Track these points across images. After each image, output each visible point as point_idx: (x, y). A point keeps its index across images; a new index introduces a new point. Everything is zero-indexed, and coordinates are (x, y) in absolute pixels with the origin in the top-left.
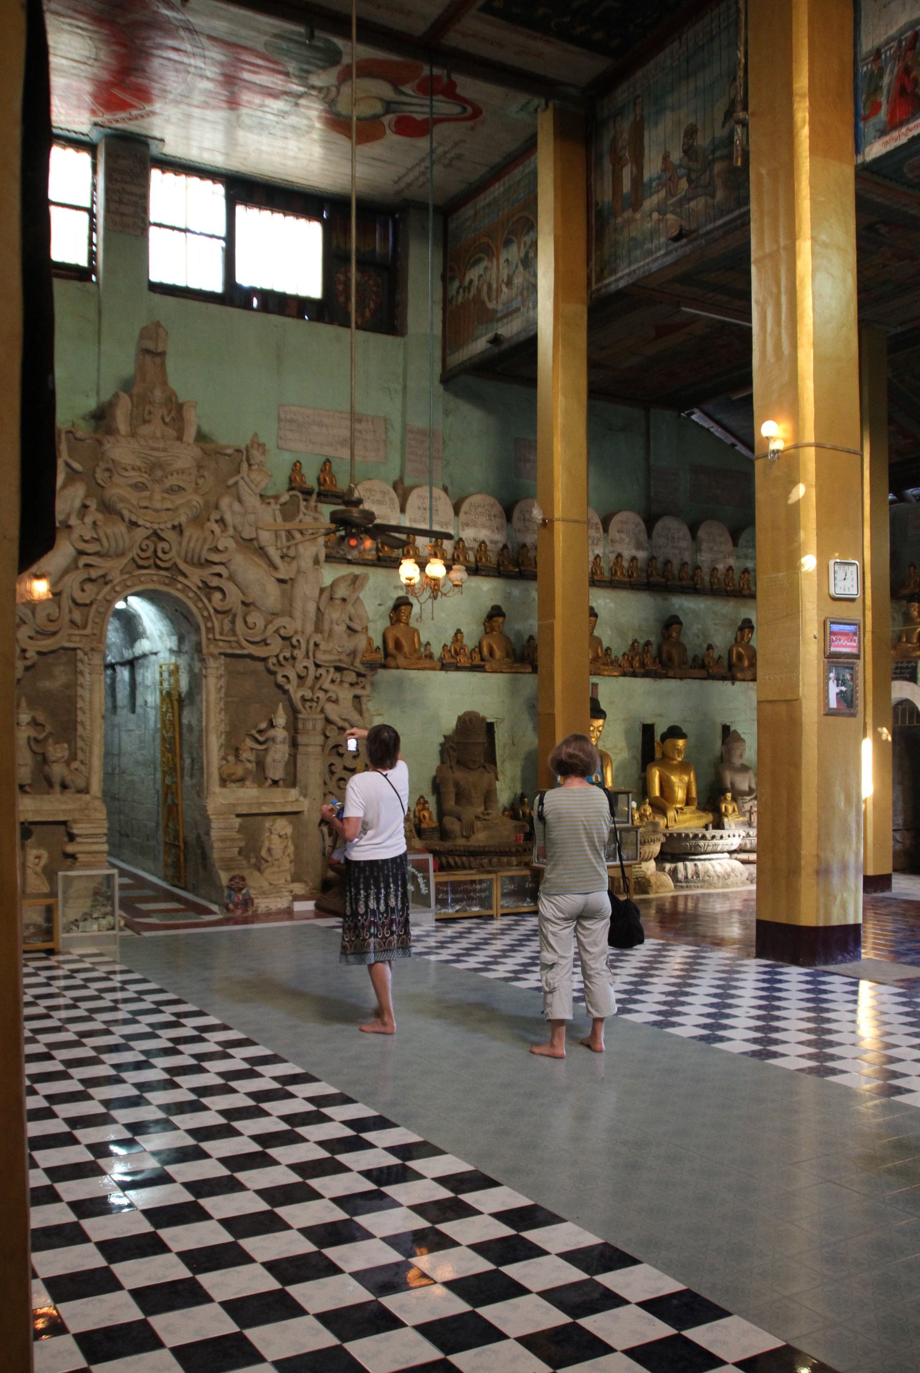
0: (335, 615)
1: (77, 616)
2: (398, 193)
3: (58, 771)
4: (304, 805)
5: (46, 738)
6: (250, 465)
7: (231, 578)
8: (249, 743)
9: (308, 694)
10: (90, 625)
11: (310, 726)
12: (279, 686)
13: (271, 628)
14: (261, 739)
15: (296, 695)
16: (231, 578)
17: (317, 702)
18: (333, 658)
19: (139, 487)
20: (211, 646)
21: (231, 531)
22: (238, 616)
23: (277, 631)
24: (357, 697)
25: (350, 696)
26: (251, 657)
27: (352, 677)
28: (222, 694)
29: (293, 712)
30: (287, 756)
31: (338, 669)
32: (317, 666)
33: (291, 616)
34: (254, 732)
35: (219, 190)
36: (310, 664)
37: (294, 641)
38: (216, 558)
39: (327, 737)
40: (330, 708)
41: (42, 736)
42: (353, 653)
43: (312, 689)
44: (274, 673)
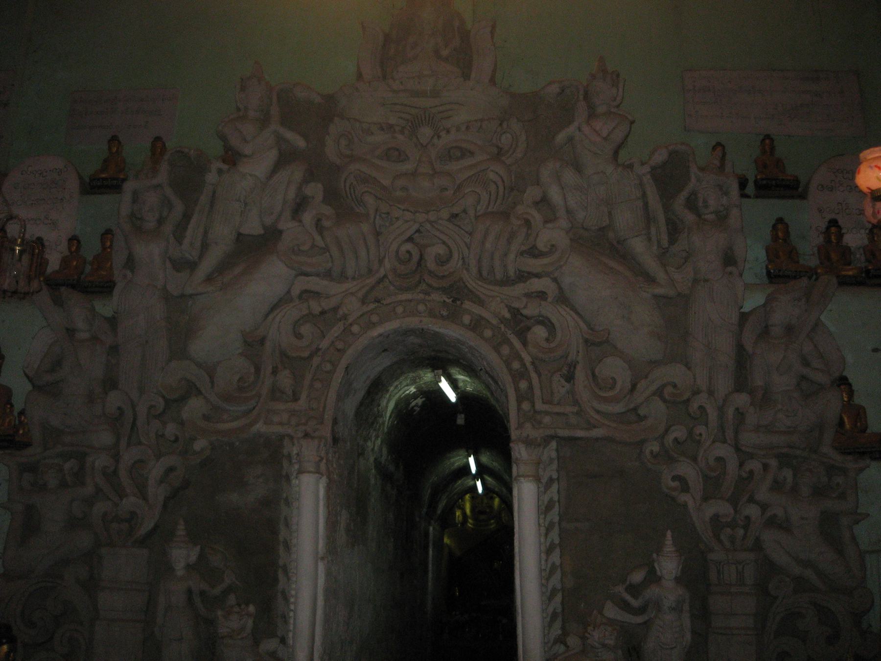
1: (285, 379)
7: (563, 299)
10: (304, 396)
14: (635, 603)
16: (563, 299)
17: (746, 527)
19: (395, 154)
20: (528, 425)
22: (579, 368)
23: (659, 393)
30: (688, 636)
34: (620, 589)
41: (217, 591)
43: (734, 501)
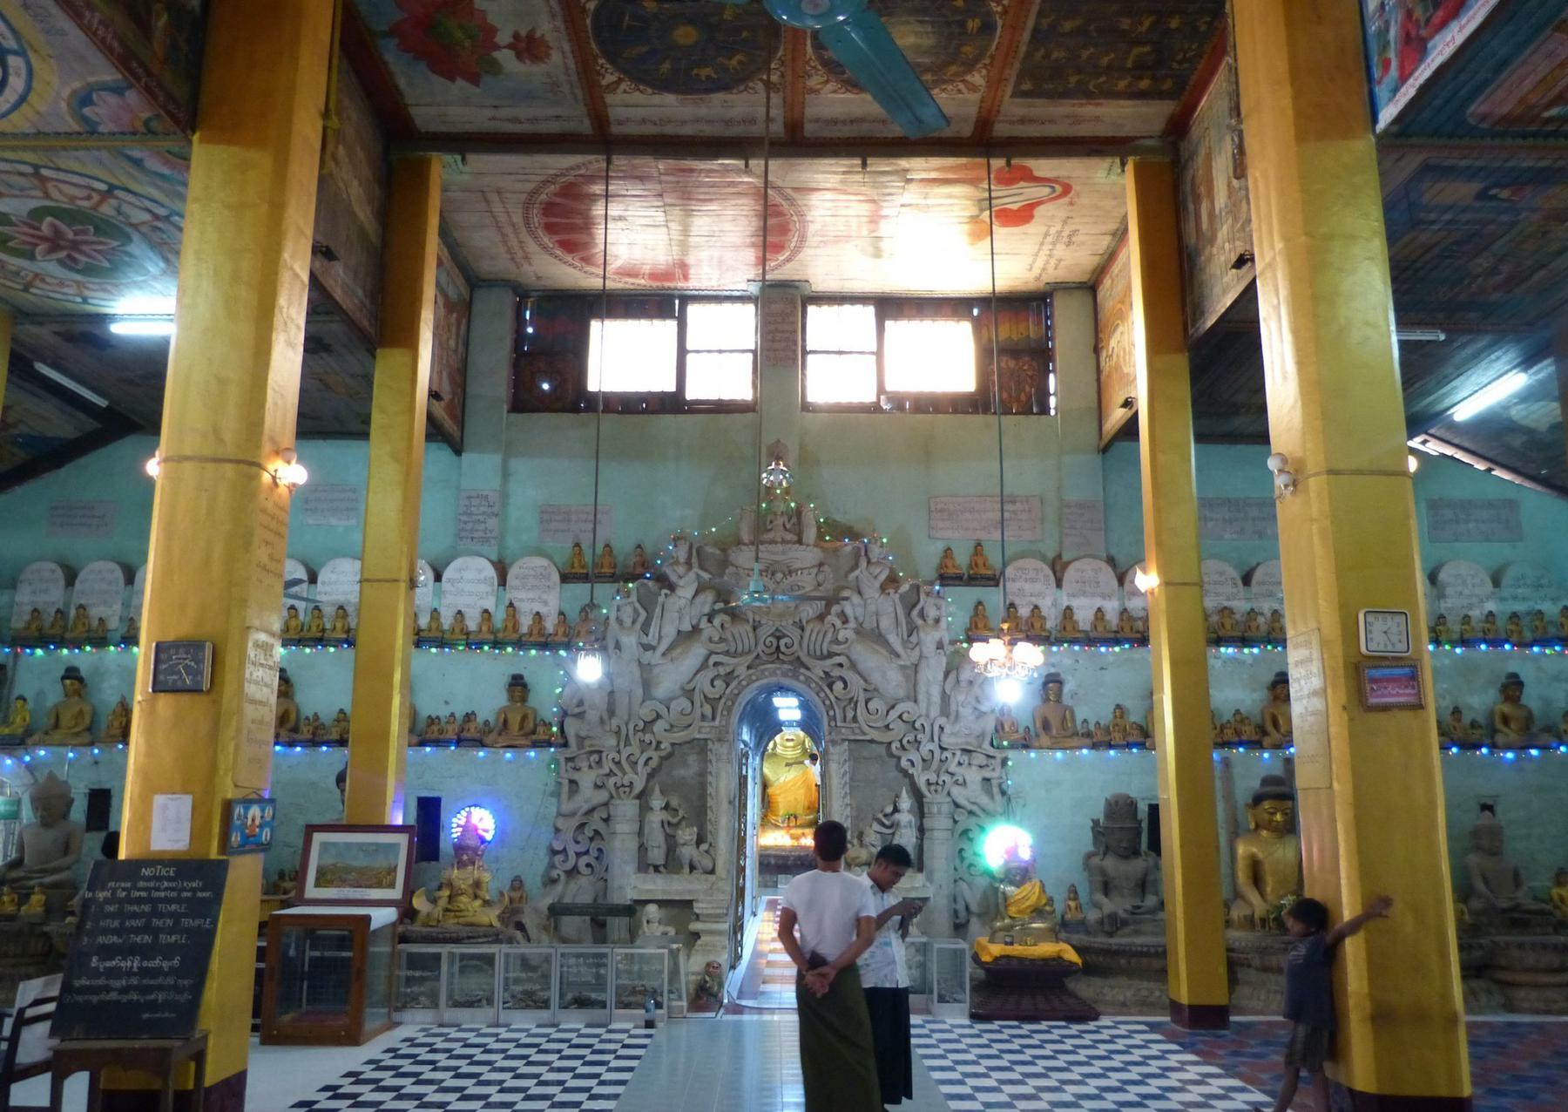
0: (961, 698)
2: (1038, 279)
3: (687, 852)
4: (929, 892)
5: (679, 823)
6: (869, 562)
7: (853, 666)
8: (876, 827)
9: (933, 779)
11: (935, 810)
12: (905, 773)
13: (894, 714)
15: (921, 781)
18: (960, 741)
21: (852, 624)
23: (900, 717)
24: (987, 780)
25: (979, 778)
26: (872, 741)
27: (982, 760)
28: (847, 778)
29: (918, 797)
31: (965, 751)
32: (942, 749)
33: (915, 701)
34: (880, 816)
35: (870, 311)
36: (934, 747)
37: (917, 725)
38: (836, 649)
39: (956, 822)
40: (957, 792)
42: (982, 735)
44: (899, 758)
